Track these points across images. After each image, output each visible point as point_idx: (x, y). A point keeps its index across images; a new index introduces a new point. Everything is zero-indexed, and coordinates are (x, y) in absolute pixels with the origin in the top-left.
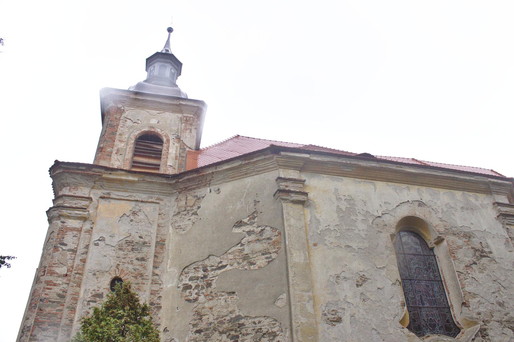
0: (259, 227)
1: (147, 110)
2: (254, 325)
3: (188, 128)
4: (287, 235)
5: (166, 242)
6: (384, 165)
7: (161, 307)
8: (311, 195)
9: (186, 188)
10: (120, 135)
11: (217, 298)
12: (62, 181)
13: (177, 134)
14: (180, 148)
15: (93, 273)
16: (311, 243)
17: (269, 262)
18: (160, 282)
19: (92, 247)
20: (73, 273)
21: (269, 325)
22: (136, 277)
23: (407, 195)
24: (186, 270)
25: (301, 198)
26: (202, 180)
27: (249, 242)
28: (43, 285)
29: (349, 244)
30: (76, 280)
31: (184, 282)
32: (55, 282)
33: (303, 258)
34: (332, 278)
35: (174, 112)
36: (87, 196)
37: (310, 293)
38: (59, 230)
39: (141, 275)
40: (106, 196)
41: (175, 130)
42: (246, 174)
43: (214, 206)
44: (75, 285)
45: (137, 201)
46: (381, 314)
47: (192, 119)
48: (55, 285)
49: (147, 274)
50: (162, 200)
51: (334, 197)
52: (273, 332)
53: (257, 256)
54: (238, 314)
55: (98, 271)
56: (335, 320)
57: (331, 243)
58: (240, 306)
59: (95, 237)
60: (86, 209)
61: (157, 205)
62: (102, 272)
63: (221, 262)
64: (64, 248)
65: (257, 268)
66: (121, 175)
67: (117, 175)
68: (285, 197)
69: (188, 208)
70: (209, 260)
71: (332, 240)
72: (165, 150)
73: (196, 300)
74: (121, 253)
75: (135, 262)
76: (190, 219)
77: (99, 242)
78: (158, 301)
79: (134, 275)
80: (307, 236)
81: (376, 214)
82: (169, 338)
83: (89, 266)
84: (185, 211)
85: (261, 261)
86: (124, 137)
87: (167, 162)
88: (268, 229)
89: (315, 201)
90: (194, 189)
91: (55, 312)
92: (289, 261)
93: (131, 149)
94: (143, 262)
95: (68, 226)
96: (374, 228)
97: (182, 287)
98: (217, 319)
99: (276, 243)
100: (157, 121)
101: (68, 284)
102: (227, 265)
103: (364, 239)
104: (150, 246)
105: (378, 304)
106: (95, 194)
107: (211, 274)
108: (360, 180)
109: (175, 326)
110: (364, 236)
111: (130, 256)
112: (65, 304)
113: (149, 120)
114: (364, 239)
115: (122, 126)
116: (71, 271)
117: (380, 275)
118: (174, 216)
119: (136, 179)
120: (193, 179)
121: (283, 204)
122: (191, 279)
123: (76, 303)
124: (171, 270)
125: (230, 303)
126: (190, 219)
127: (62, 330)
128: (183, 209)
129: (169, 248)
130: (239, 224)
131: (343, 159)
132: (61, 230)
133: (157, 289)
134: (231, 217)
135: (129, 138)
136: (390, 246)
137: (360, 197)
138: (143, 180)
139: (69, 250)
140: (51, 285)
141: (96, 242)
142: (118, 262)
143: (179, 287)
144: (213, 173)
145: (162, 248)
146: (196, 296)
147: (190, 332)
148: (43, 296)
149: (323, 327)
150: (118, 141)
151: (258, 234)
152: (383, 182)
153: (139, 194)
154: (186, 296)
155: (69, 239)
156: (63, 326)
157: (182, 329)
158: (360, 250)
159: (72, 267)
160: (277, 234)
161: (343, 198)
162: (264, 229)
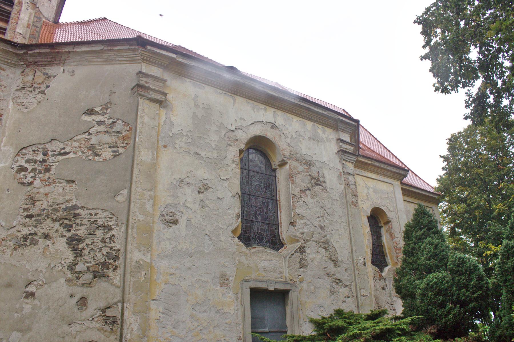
0: (111, 118)
4: (138, 131)
8: (170, 97)
11: (54, 185)
14: (35, 16)
17: (115, 156)
26: (55, 57)
27: (98, 132)
29: (198, 151)
31: (19, 163)
33: (150, 157)
34: (175, 181)
37: (152, 193)
42: (106, 61)
43: (66, 88)
52: (108, 225)
53: (104, 148)
54: (74, 203)
57: (181, 147)
58: (78, 196)
63: (64, 148)
65: (101, 160)
68: (142, 93)
70: (51, 144)
71: (182, 144)
72: (16, 14)
76: (35, 98)
80: (158, 137)
81: (230, 128)
84: (30, 87)
87: (16, 28)
88: (120, 122)
89: (173, 103)
90: (45, 65)
92: (136, 158)
97: (16, 168)
98: (51, 206)
99: (125, 138)
102: (70, 152)
103: (214, 149)
107: (51, 159)
110: (214, 146)
114: (214, 149)
117: (222, 186)
118: (17, 90)
120: (46, 54)
121: (140, 99)
122: (28, 161)
124: (5, 149)
125: (67, 191)
126: (35, 98)
128: (29, 85)
129: (7, 125)
130: (90, 112)
134: (82, 104)
136: (237, 161)
143: (12, 168)
144: (69, 52)
147: (19, 216)
149: (158, 226)
151: (108, 125)
152: (242, 98)
154: (20, 179)
157: (11, 212)
158: (208, 158)
160: (128, 129)
161: (201, 106)
162: (116, 122)
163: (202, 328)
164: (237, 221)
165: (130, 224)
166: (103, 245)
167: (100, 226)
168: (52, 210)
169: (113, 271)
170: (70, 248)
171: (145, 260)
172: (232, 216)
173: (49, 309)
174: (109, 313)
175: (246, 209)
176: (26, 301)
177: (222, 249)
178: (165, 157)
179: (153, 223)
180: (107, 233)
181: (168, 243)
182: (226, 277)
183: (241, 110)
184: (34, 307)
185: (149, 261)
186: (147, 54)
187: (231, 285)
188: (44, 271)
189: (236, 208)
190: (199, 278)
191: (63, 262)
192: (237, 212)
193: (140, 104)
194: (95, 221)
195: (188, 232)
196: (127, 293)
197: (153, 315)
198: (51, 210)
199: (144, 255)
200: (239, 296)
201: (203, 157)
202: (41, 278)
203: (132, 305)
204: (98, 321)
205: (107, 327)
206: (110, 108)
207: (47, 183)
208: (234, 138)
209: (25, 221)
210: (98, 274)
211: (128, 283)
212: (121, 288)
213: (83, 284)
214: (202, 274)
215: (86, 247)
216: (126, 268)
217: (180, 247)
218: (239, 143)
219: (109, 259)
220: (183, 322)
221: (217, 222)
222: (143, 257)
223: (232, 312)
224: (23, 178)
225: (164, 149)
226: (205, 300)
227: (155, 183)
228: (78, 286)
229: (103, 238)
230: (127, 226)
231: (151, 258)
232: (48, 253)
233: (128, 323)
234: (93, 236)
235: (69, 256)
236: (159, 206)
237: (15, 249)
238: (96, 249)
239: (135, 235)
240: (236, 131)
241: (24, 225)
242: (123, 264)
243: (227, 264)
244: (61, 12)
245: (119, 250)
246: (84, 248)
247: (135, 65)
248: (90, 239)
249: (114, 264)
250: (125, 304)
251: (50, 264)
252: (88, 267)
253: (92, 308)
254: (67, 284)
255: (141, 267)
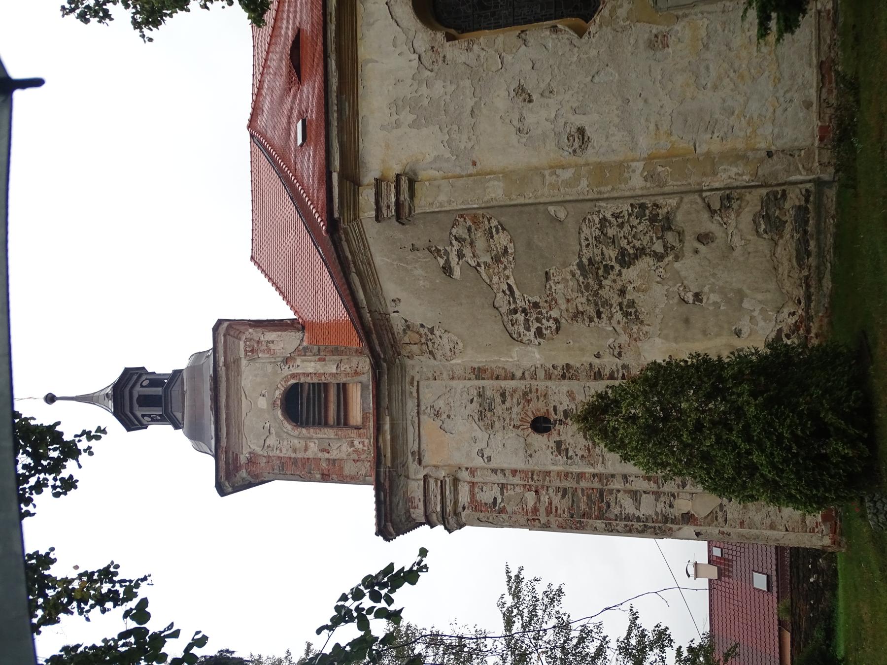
0: (451, 243)
1: (244, 415)
2: (591, 246)
3: (265, 348)
4: (464, 207)
5: (476, 365)
6: (332, 46)
7: (567, 364)
8: (397, 169)
9: (392, 346)
10: (295, 451)
11: (554, 294)
12: (403, 520)
13: (279, 363)
14: (305, 355)
15: (529, 458)
16: (471, 170)
17: (503, 229)
18: (533, 368)
19: (494, 464)
20: (533, 483)
21: (590, 228)
22: (529, 401)
23: (377, 5)
24: (515, 336)
25: (404, 186)
26: (380, 326)
27: (474, 256)
28: (552, 519)
29: (469, 112)
30: (541, 478)
31: (532, 338)
32: (547, 504)
33: (496, 183)
34: (521, 140)
35: (239, 373)
36: (422, 482)
37: (547, 173)
38: (476, 511)
39: (525, 394)
40: (417, 457)
41: (273, 368)
42: (369, 264)
43: (420, 305)
44: (547, 478)
45: (418, 413)
46: (571, 68)
47: (248, 343)
48: (551, 503)
49: (523, 387)
50: (413, 378)
51: (395, 131)
52: (600, 223)
53: (495, 245)
54: (575, 267)
55: (526, 452)
56: (581, 138)
57: (469, 139)
58: (565, 265)
59: (479, 462)
60: (442, 482)
61: (421, 383)
62: (528, 446)
63: (504, 292)
64: (499, 500)
65: (512, 245)
66: (384, 441)
67: (385, 445)
68: (407, 210)
69: (423, 340)
70: (501, 307)
71: (465, 137)
72: (312, 378)
73: (557, 321)
74: (497, 425)
75: (508, 404)
76: (441, 337)
77: (485, 456)
78: (559, 369)
79: (526, 404)
80: (463, 176)
81: (416, 62)
82: (608, 350)
83: (520, 465)
84: (427, 345)
85: (502, 239)
86: (298, 446)
87: (332, 374)
88: (454, 231)
89: (405, 162)
90: (393, 334)
91: (585, 497)
92: (502, 203)
93: (318, 431)
94: (507, 394)
95: (469, 500)
96: (439, 69)
97: (539, 340)
98: (582, 293)
99: (475, 220)
100: (261, 397)
101: (548, 487)
102: (507, 283)
103: (458, 86)
104: (483, 387)
105: (556, 70)
106: (416, 472)
107: (520, 304)
108: (360, 88)
109: (592, 344)
110: (453, 87)
111: (500, 413)
112: (574, 487)
113: (261, 410)
114: (458, 86)
115: (278, 451)
116: (530, 486)
117: (513, 64)
118: (435, 359)
119: (388, 419)
120: (380, 338)
121: (416, 212)
122: (528, 329)
123: (572, 473)
124: (515, 356)
125: (560, 278)
126: (441, 337)
127: (606, 485)
128: (425, 347)
129: (484, 360)
130: (447, 270)
131: (331, 118)
132: (475, 508)
133: (544, 372)
134: (438, 281)
135: (298, 438)
136: (466, 44)
137: (391, 88)
138: (388, 408)
139: (502, 493)
140: (551, 508)
141: (486, 460)
142: (511, 427)
143: (540, 344)
144: (370, 311)
145: (485, 370)
146: (551, 321)
147: (600, 325)
148: (566, 515)
149: (591, 155)
150: (307, 453)
151: (462, 244)
152: (359, 47)
153: (408, 412)
154: (552, 333)
155: (486, 496)
156: (602, 485)
157: (596, 335)
158: (475, 94)
159: (525, 486)
160: (462, 219)
161: (395, 117)
162: (455, 236)
163: (732, 71)
164: (563, 32)
165: (596, 196)
166: (627, 225)
167: (602, 232)
168: (587, 291)
169: (661, 207)
170: (634, 262)
171: (641, 169)
172: (556, 41)
173: (714, 275)
174: (716, 206)
175: (539, 11)
176: (705, 300)
177: (611, 51)
178: (492, 161)
179: (588, 165)
180: (610, 222)
181: (613, 138)
182: (653, 39)
183: (380, 47)
184: (712, 291)
185: (643, 163)
186: (346, 215)
187: (663, 28)
188: (666, 287)
189: (543, 35)
190: (658, 85)
191: (654, 268)
192: (548, 33)
193: (424, 211)
194: (596, 239)
195: (593, 110)
196: (688, 188)
197: (716, 147)
198: (588, 292)
199: (634, 171)
200: (680, 13)
201: (476, 103)
202: (676, 289)
203: (704, 179)
204: (727, 217)
205: (735, 205)
206: (436, 247)
207: (554, 302)
208: (431, 53)
209: (605, 318)
210: (666, 225)
211: (675, 187)
212: (683, 195)
213: (680, 241)
214: (651, 81)
215: (632, 245)
216: (656, 193)
217: (616, 120)
218: (437, 44)
219: (645, 215)
220: (724, 101)
221: (570, 65)
222: (638, 172)
223: (706, 22)
224: (551, 330)
225: (478, 164)
226: (690, 71)
227: (531, 170)
228: (683, 246)
229: (617, 226)
230: (598, 200)
231: (638, 161)
232: (644, 286)
233: (729, 181)
234: (615, 238)
235: (645, 263)
236: (562, 158)
237: (642, 322)
238: (633, 233)
239: (609, 188)
240: (418, 50)
241: (610, 318)
242: (650, 197)
243: (632, 41)
244: (267, 321)
245: (632, 205)
246: (634, 247)
247: (364, 227)
248: (621, 242)
249: (651, 209)
250: (704, 188)
251: (658, 282)
252: (658, 238)
253: (712, 227)
254: (682, 259)
255: (652, 173)
